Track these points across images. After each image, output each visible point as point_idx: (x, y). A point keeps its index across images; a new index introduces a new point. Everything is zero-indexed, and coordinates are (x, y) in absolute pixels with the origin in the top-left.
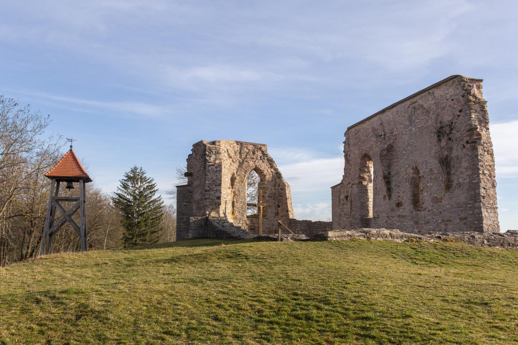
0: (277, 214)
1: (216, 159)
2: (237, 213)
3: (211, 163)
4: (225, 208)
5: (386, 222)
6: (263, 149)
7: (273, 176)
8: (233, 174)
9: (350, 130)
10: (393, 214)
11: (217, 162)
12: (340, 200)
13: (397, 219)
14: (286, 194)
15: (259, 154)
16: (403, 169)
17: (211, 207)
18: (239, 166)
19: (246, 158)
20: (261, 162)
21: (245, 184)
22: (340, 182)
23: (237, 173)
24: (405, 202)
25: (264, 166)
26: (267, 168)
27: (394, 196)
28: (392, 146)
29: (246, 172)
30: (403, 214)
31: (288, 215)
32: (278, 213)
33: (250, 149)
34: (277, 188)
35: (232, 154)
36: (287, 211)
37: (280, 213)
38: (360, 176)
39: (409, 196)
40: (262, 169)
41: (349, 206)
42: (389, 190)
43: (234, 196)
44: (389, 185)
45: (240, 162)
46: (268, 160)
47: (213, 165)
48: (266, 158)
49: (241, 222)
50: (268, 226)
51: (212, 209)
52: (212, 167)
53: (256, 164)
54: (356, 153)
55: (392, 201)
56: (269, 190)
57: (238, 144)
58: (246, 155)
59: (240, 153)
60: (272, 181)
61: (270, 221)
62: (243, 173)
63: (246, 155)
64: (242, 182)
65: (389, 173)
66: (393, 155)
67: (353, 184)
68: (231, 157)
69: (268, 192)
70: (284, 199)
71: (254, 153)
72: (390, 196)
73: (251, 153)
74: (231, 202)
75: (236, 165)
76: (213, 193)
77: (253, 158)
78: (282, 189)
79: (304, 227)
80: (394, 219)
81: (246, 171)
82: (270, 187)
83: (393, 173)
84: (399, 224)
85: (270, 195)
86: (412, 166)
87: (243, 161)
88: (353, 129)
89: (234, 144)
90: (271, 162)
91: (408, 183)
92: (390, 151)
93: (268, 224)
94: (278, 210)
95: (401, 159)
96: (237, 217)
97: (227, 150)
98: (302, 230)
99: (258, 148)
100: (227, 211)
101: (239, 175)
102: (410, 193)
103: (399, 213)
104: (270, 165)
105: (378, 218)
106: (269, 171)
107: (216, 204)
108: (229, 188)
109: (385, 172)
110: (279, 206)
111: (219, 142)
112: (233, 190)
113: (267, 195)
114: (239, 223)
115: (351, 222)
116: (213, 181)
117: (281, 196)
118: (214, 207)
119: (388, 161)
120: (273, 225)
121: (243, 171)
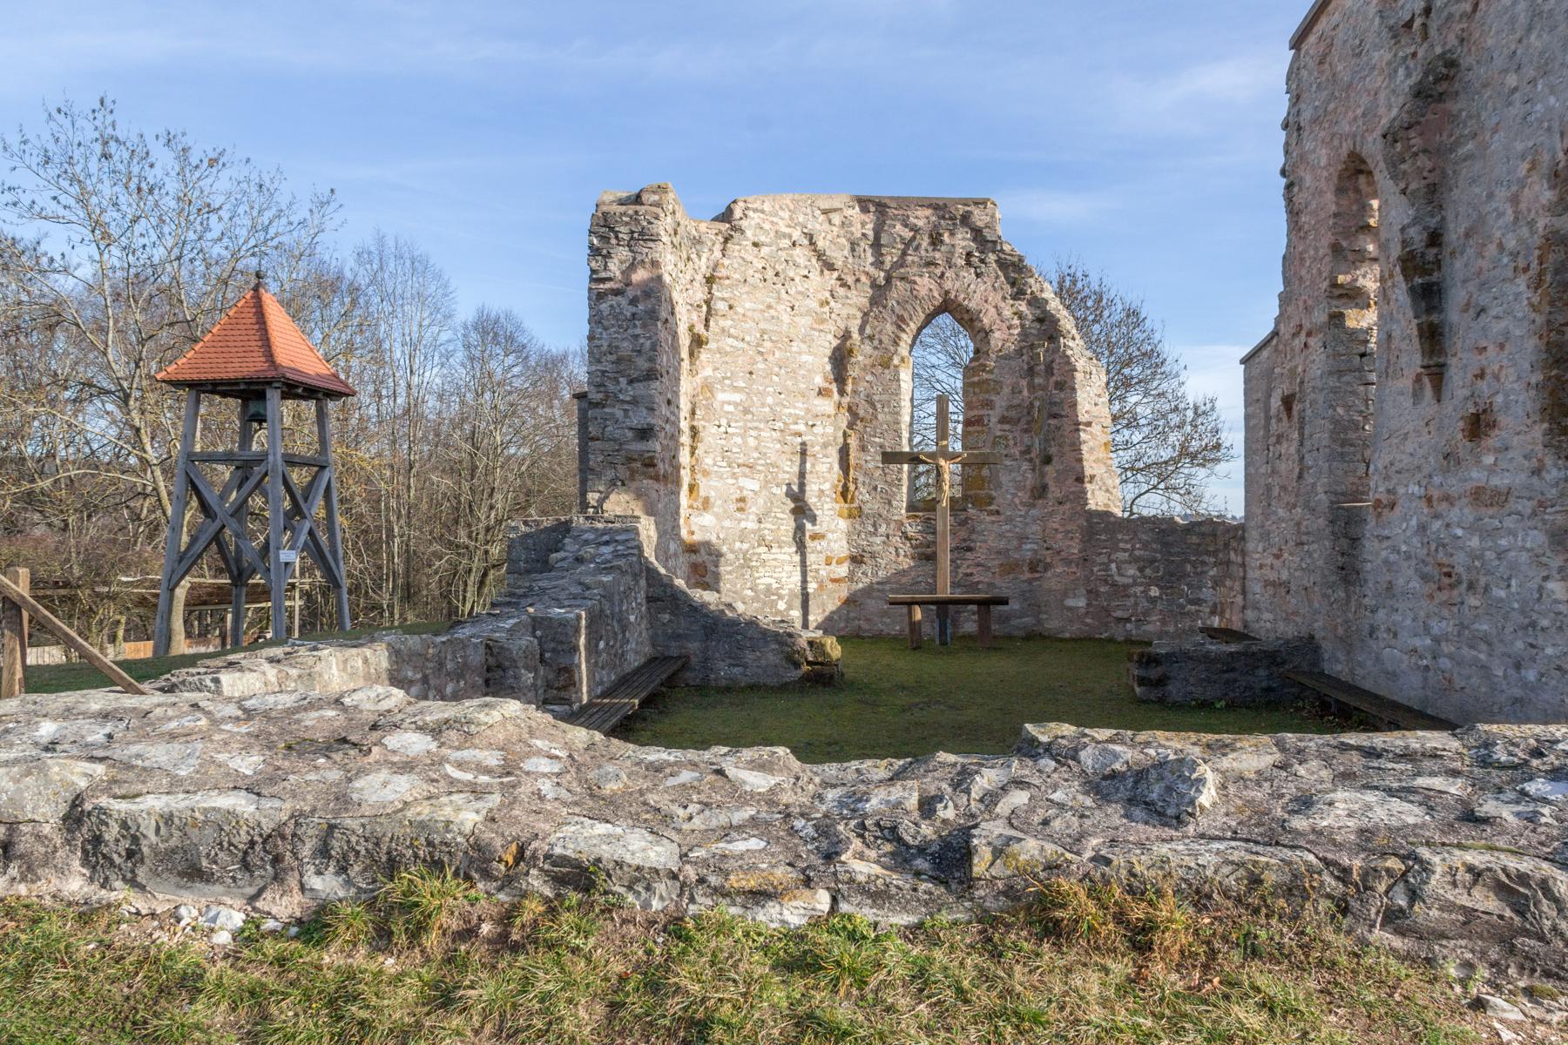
0: (1040, 491)
1: (632, 267)
2: (863, 494)
3: (608, 285)
4: (802, 475)
5: (1422, 528)
6: (979, 217)
7: (1024, 334)
8: (846, 335)
9: (1304, 47)
10: (1454, 485)
11: (640, 275)
12: (1268, 418)
13: (1469, 514)
14: (1074, 405)
15: (962, 241)
16: (1502, 193)
17: (610, 474)
18: (874, 301)
19: (901, 263)
20: (969, 275)
21: (897, 374)
22: (1269, 328)
23: (862, 330)
24: (1507, 406)
25: (984, 294)
26: (995, 298)
27: (1458, 378)
28: (1452, 64)
29: (900, 322)
30: (1496, 481)
31: (1081, 497)
32: (1044, 488)
33: (920, 223)
34: (1038, 381)
35: (839, 256)
36: (1080, 479)
37: (1052, 487)
38: (1334, 285)
39: (1527, 366)
40: (972, 305)
41: (1292, 450)
42: (1433, 337)
43: (851, 426)
44: (1430, 310)
45: (874, 285)
46: (1002, 264)
47: (617, 292)
48: (992, 257)
49: (883, 529)
50: (1002, 545)
51: (613, 484)
52: (612, 300)
53: (948, 285)
54: (1323, 158)
55: (1448, 407)
56: (1006, 390)
57: (865, 210)
58: (904, 253)
59: (877, 245)
60: (1019, 353)
61: (1010, 520)
62: (889, 328)
63: (904, 253)
64: (886, 364)
65: (1435, 238)
66: (1453, 118)
67: (1309, 334)
68: (830, 267)
69: (1000, 402)
70: (1068, 429)
71: (936, 241)
72: (1436, 374)
73: (925, 243)
74: (833, 453)
75: (859, 298)
76: (619, 414)
77: (931, 263)
78: (1060, 386)
79: (1145, 546)
80: (1454, 514)
81: (901, 318)
82: (1008, 380)
83: (1454, 234)
84: (1475, 542)
85: (1013, 414)
86: (1546, 158)
87: (888, 279)
88: (1312, 39)
89: (849, 212)
90: (1014, 271)
91: (1522, 283)
92: (1441, 97)
93: (1001, 536)
94: (1042, 475)
95: (1495, 131)
96: (866, 509)
97: (810, 237)
98: (1136, 560)
99: (951, 214)
100: (812, 489)
101: (871, 338)
102: (1532, 343)
103: (1477, 476)
104: (1013, 284)
105: (1392, 506)
106: (1007, 313)
107: (630, 460)
108: (821, 392)
109: (1412, 232)
110: (1048, 460)
111: (662, 189)
112: (846, 400)
113: (993, 417)
114: (875, 534)
115: (1298, 524)
116: (619, 361)
117: (1055, 416)
118: (623, 472)
119: (1424, 161)
120: (1023, 538)
121: (890, 318)
